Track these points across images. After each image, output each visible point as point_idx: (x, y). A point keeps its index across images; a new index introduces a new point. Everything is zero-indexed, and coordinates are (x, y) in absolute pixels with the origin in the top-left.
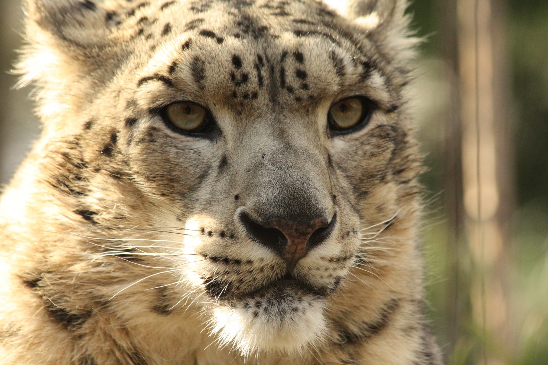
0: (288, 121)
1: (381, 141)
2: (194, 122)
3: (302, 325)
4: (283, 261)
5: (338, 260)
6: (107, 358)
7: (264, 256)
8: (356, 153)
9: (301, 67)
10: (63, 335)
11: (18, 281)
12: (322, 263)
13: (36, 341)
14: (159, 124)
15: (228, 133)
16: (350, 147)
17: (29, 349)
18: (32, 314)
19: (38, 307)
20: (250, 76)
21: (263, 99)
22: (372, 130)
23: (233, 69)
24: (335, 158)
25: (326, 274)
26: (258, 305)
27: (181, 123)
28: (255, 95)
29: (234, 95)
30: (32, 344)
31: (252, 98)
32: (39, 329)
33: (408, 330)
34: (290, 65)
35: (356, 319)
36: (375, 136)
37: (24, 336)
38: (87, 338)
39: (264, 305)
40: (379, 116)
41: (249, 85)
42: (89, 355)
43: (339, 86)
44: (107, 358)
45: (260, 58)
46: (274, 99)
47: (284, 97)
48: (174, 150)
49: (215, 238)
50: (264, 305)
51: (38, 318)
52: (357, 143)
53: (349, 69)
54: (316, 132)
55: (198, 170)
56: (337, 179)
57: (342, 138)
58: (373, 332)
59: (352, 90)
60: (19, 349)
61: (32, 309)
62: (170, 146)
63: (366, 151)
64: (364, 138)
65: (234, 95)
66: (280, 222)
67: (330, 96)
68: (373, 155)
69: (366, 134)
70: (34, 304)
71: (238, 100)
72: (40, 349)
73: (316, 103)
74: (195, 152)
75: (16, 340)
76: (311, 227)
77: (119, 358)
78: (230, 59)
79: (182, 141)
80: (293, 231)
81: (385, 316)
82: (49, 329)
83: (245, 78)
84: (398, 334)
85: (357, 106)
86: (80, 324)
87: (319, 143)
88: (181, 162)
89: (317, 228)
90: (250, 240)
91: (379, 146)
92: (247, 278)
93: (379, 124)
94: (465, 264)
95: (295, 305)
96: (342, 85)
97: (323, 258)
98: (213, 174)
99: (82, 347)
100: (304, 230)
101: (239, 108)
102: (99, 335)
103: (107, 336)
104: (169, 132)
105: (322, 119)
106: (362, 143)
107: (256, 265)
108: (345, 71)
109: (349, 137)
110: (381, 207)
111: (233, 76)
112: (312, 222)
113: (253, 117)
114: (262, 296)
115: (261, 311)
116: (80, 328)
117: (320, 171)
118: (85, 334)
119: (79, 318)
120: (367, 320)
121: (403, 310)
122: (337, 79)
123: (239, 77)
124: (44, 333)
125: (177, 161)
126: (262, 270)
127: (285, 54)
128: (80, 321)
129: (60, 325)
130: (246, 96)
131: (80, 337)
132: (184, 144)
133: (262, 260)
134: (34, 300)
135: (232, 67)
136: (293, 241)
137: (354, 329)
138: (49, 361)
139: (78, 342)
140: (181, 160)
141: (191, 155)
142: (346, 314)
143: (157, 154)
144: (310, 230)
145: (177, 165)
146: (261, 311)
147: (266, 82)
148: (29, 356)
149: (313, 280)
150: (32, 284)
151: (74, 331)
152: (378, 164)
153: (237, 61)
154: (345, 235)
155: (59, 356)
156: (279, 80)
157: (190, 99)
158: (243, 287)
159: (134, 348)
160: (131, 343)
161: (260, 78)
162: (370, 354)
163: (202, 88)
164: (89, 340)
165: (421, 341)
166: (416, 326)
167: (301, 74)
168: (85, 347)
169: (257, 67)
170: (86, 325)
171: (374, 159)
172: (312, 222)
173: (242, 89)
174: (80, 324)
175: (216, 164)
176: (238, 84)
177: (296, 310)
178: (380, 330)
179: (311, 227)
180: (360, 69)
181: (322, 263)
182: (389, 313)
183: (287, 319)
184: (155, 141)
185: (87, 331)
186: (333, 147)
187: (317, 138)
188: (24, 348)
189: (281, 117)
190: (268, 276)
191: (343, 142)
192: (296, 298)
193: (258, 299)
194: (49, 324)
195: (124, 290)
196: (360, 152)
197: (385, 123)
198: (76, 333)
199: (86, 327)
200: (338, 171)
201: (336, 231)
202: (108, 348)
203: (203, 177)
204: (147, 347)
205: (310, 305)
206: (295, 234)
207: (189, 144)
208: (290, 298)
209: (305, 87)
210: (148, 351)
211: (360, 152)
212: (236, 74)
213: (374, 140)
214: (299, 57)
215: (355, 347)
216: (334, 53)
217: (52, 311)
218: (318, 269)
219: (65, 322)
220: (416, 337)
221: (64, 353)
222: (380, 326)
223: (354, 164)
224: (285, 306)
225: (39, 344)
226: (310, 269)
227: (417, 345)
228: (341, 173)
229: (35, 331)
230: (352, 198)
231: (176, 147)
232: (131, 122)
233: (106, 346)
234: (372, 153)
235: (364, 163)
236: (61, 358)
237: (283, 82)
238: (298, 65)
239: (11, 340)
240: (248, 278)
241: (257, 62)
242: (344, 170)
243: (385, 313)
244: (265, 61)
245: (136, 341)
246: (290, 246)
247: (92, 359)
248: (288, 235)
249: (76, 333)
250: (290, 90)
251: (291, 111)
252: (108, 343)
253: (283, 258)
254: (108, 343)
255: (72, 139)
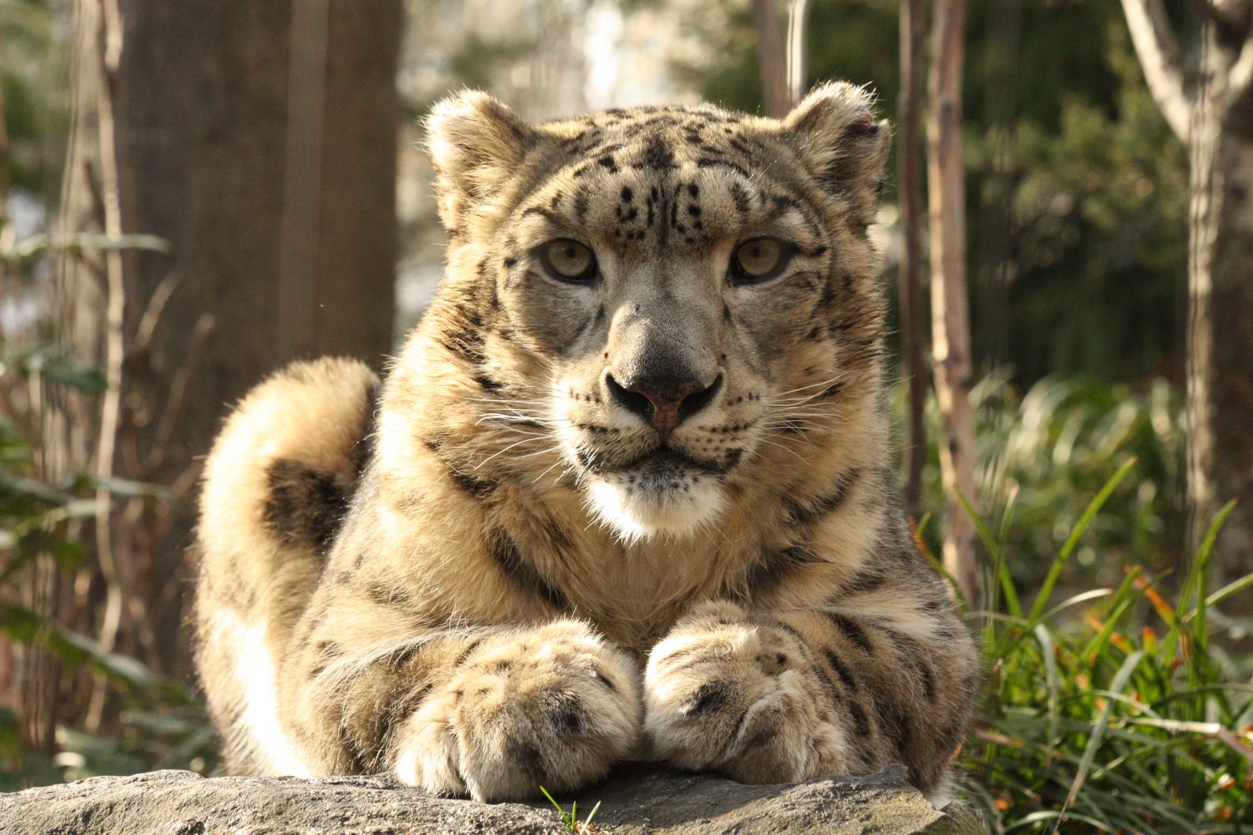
0: (675, 266)
1: (798, 290)
2: (578, 268)
3: (685, 505)
4: (654, 430)
5: (725, 430)
6: (522, 530)
7: (630, 424)
8: (765, 305)
9: (695, 203)
10: (471, 503)
11: (419, 444)
12: (701, 433)
13: (441, 510)
14: (538, 270)
15: (609, 278)
16: (759, 298)
17: (433, 519)
18: (435, 479)
19: (442, 472)
20: (639, 212)
21: (651, 240)
22: (789, 278)
23: (620, 203)
24: (734, 312)
25: (709, 446)
26: (632, 480)
27: (564, 269)
28: (641, 235)
29: (617, 233)
30: (436, 514)
31: (638, 238)
32: (443, 497)
33: (870, 505)
34: (684, 201)
35: (808, 492)
36: (791, 285)
37: (427, 504)
38: (498, 507)
39: (638, 480)
40: (798, 261)
41: (636, 223)
42: (502, 527)
43: (740, 223)
44: (522, 530)
45: (654, 191)
46: (662, 241)
47: (675, 238)
48: (552, 299)
49: (582, 402)
50: (638, 480)
51: (443, 484)
52: (768, 293)
53: (755, 204)
54: (711, 282)
55: (577, 322)
56: (735, 335)
57: (749, 287)
58: (828, 509)
59: (758, 230)
60: (423, 519)
61: (435, 474)
62: (549, 294)
63: (779, 302)
64: (778, 288)
65: (617, 233)
66: (643, 385)
67: (730, 235)
68: (786, 307)
69: (780, 283)
70: (438, 469)
71: (621, 240)
72: (447, 518)
73: (712, 244)
74: (575, 301)
75: (420, 509)
76: (682, 392)
77: (535, 530)
78: (619, 192)
79: (561, 289)
80: (658, 396)
81: (842, 489)
82: (455, 496)
83: (633, 214)
84: (859, 510)
85: (773, 250)
86: (489, 491)
87: (712, 293)
88: (560, 313)
89: (688, 393)
90: (615, 405)
91: (795, 297)
92: (616, 449)
93: (798, 270)
94: (320, 477)
95: (676, 480)
96: (744, 222)
97: (701, 428)
98: (590, 326)
99: (493, 517)
100: (672, 395)
101: (622, 250)
102: (511, 504)
103: (520, 507)
104: (547, 278)
105: (720, 264)
106: (774, 294)
107: (623, 434)
108: (749, 205)
109: (757, 287)
110: (812, 370)
111: (618, 211)
112: (681, 386)
113: (637, 261)
114: (638, 469)
115: (635, 486)
116: (488, 496)
117: (703, 326)
118: (495, 503)
119: (488, 485)
120: (821, 493)
121: (864, 481)
122: (737, 215)
123: (625, 212)
124: (449, 501)
125: (555, 311)
126: (631, 441)
127: (679, 188)
128: (488, 489)
129: (467, 493)
130: (630, 235)
131: (491, 506)
132: (564, 292)
133: (629, 429)
134: (439, 464)
135: (619, 200)
136: (660, 408)
137: (806, 505)
138: (456, 533)
139: (489, 512)
140: (559, 311)
141: (571, 304)
142: (792, 489)
143: (533, 303)
144: (679, 395)
145: (554, 315)
146: (635, 486)
147: (657, 219)
148: (433, 527)
149: (693, 453)
150: (432, 447)
151: (482, 500)
152: (794, 318)
153: (627, 194)
154: (734, 401)
155: (467, 527)
156: (670, 217)
157: (570, 236)
158: (615, 459)
159: (551, 519)
160: (547, 513)
161: (651, 215)
162: (825, 533)
163: (583, 223)
164: (501, 509)
165: (885, 517)
166: (880, 499)
167: (694, 211)
168: (496, 517)
169: (649, 203)
170: (495, 493)
171: (787, 312)
172: (681, 386)
173: (630, 226)
174: (489, 491)
175: (594, 315)
176: (623, 220)
177: (676, 486)
178: (836, 505)
179: (682, 392)
180: (769, 205)
181: (701, 433)
182: (847, 485)
183: (666, 498)
184: (532, 288)
185: (497, 499)
186: (736, 298)
187: (711, 287)
188: (428, 517)
189: (668, 262)
190: (639, 447)
191: (751, 293)
192: (677, 472)
193: (634, 473)
194: (455, 490)
195: (542, 456)
196: (770, 304)
197: (806, 270)
198: (484, 502)
199: (496, 495)
200: (738, 326)
201: (720, 397)
202: (522, 519)
203: (581, 329)
204: (567, 518)
205: (695, 480)
206: (660, 399)
207: (568, 292)
208: (668, 473)
209: (698, 225)
210: (569, 523)
211: (770, 304)
212: (622, 208)
213: (789, 290)
214: (694, 190)
215: (808, 525)
216: (737, 185)
217: (456, 477)
218: (698, 440)
219: (472, 489)
220: (880, 512)
221: (473, 524)
222: (837, 501)
223: (762, 318)
224: (662, 481)
225: (445, 513)
226: (687, 440)
227: (880, 522)
228: (744, 329)
229: (440, 499)
230: (755, 358)
231: (555, 295)
232: (510, 263)
233: (519, 517)
234: (785, 305)
235: (774, 318)
236: (470, 529)
237: (674, 220)
238: (691, 199)
239: (414, 508)
240: (618, 449)
241: (651, 197)
242: (748, 325)
243: (842, 485)
244: (660, 195)
245: (554, 513)
246: (657, 415)
247: (505, 532)
248: (653, 400)
249: (484, 502)
250: (682, 229)
251: (682, 255)
252: (521, 513)
253: (653, 427)
254: (521, 513)
255: (466, 286)
